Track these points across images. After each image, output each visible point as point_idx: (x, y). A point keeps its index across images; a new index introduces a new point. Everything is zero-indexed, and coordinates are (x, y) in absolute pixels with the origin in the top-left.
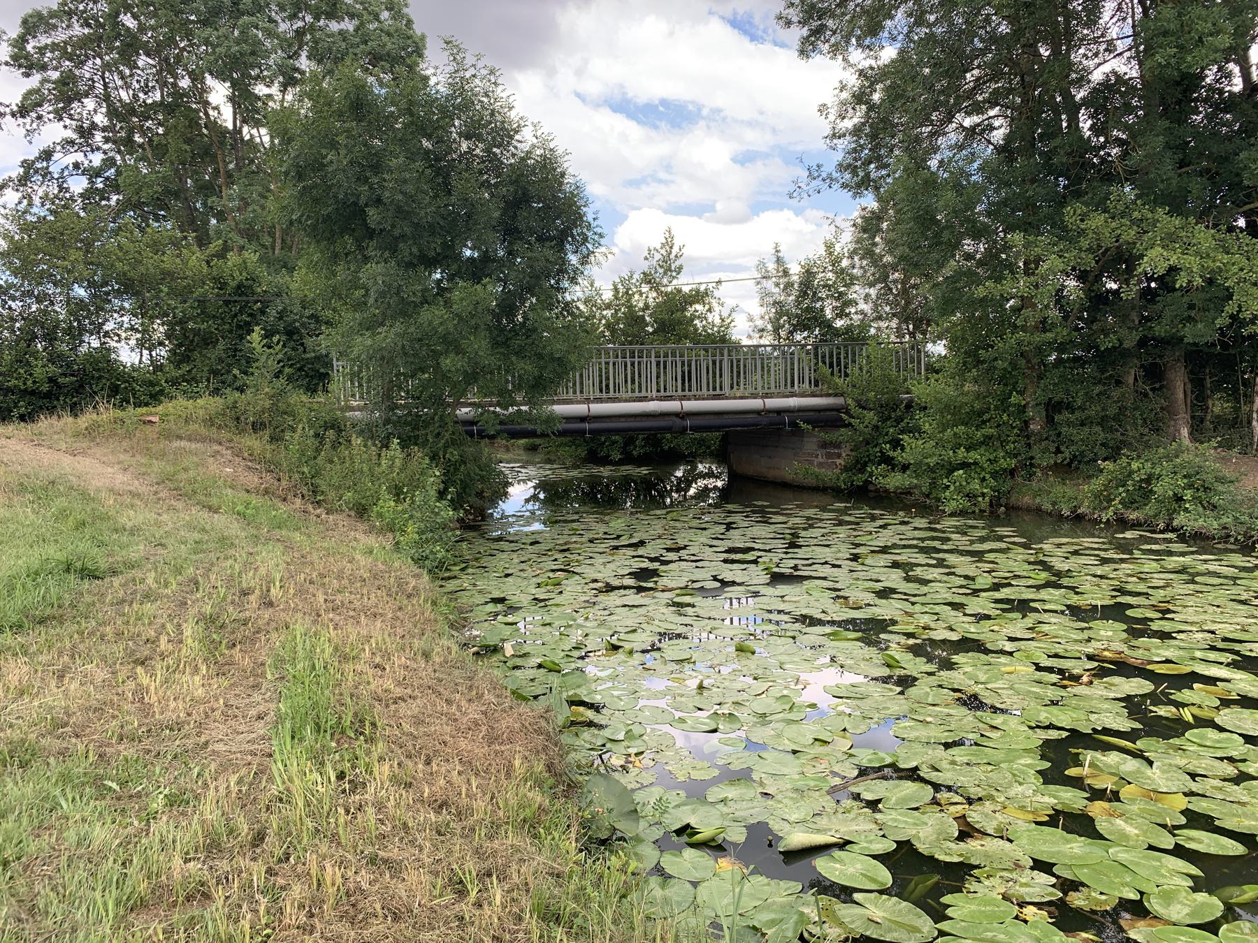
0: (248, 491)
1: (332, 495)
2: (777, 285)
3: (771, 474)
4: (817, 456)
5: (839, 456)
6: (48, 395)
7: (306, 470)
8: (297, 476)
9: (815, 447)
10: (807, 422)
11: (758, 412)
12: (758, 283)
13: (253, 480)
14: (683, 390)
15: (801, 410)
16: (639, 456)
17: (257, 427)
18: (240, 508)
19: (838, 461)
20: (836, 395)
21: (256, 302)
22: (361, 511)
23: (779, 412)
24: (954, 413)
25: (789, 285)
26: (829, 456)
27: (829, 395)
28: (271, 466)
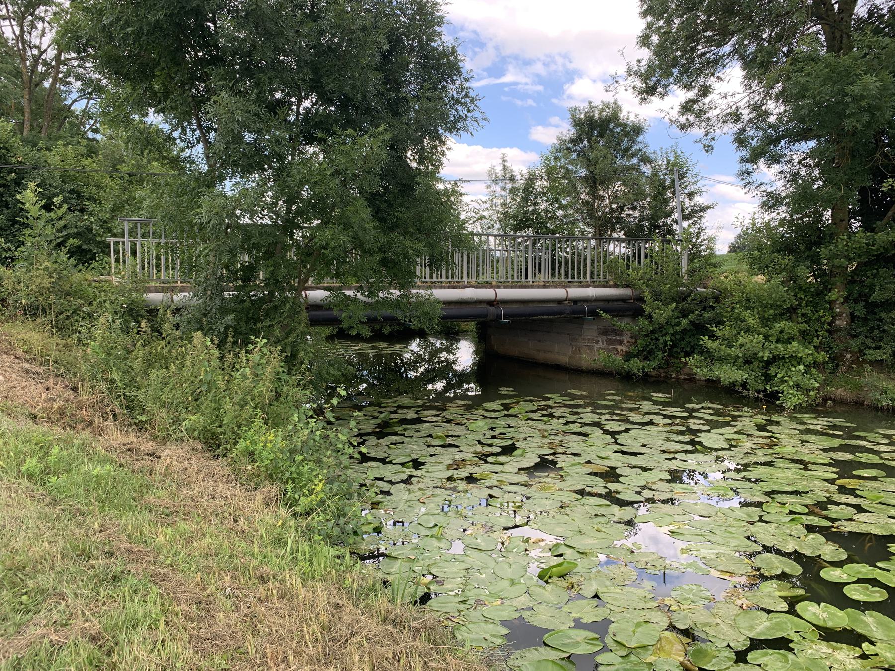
0: (34, 417)
1: (163, 416)
2: (504, 189)
3: (542, 357)
4: (597, 342)
5: (621, 343)
6: (776, 141)
7: (116, 376)
8: (104, 385)
9: (595, 334)
10: (606, 311)
11: (559, 301)
12: (489, 187)
13: (35, 393)
14: (447, 278)
15: (598, 300)
16: (391, 333)
17: (33, 311)
18: (31, 464)
19: (619, 348)
20: (628, 286)
21: (10, 173)
22: (213, 443)
23: (575, 301)
24: (774, 311)
25: (513, 191)
26: (610, 342)
27: (616, 286)
28: (62, 369)
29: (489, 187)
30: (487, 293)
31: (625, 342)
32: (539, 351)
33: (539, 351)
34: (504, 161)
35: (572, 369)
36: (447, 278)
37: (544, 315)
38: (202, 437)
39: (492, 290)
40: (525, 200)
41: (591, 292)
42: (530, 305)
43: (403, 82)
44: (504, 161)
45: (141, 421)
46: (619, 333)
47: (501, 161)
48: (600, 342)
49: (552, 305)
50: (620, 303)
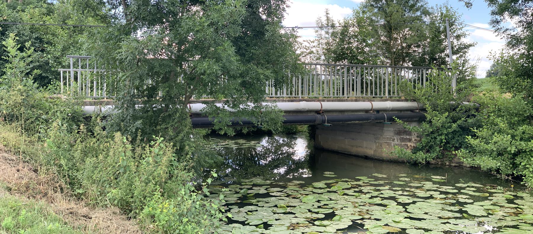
3: (354, 150)
4: (394, 140)
5: (410, 140)
9: (392, 134)
11: (367, 111)
19: (409, 144)
26: (403, 140)
27: (406, 100)
29: (317, 31)
31: (413, 140)
32: (353, 146)
33: (353, 146)
34: (327, 14)
35: (376, 159)
38: (119, 204)
40: (342, 40)
44: (327, 14)
46: (409, 133)
47: (325, 14)
48: (396, 140)
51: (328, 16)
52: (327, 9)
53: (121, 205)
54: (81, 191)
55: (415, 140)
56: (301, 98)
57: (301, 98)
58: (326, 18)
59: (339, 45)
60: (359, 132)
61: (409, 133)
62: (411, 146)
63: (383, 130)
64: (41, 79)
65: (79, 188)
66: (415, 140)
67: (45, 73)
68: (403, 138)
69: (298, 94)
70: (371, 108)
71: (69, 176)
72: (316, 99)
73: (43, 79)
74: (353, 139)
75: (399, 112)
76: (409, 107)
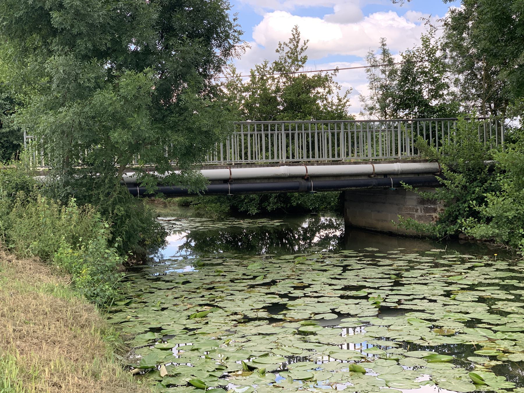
3: (380, 226)
4: (417, 211)
5: (435, 210)
9: (415, 203)
10: (408, 182)
11: (368, 175)
12: (368, 71)
19: (434, 215)
22: (45, 257)
23: (386, 175)
26: (427, 210)
27: (426, 161)
29: (368, 71)
30: (367, 168)
31: (439, 209)
32: (378, 220)
33: (378, 220)
34: (383, 45)
35: (399, 235)
36: (333, 156)
37: (351, 186)
38: (40, 254)
39: (304, 167)
40: (405, 79)
41: (397, 167)
42: (342, 178)
43: (192, 16)
44: (383, 45)
45: (11, 248)
46: (433, 202)
47: (380, 45)
48: (419, 211)
49: (363, 178)
50: (412, 176)
51: (385, 47)
52: (383, 39)
53: (42, 255)
54: (13, 246)
55: (442, 210)
56: (222, 164)
57: (222, 164)
58: (382, 51)
59: (400, 86)
60: (384, 203)
61: (433, 202)
62: (436, 217)
63: (405, 198)
64: (13, 147)
65: (12, 244)
66: (442, 210)
67: (17, 140)
68: (427, 208)
69: (339, 155)
70: (372, 171)
71: (5, 235)
72: (366, 162)
73: (15, 148)
74: (379, 212)
75: (417, 176)
76: (426, 169)
